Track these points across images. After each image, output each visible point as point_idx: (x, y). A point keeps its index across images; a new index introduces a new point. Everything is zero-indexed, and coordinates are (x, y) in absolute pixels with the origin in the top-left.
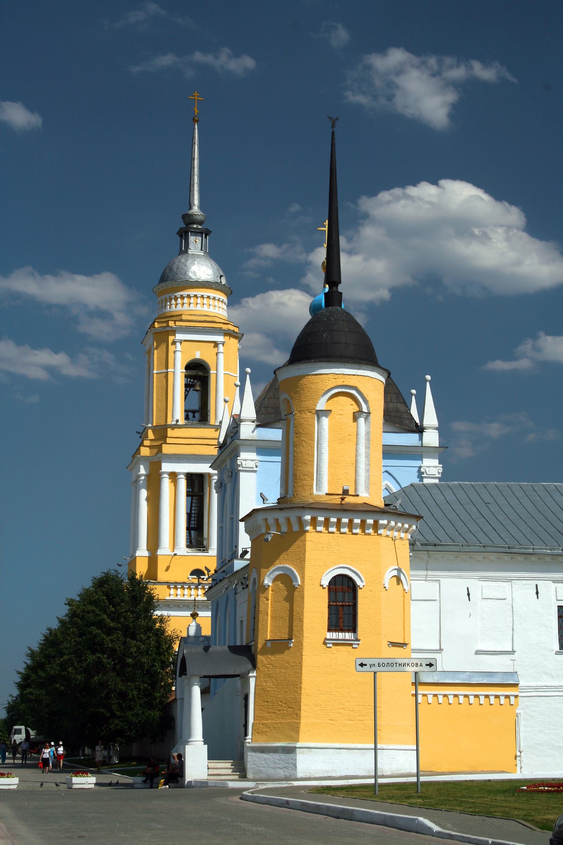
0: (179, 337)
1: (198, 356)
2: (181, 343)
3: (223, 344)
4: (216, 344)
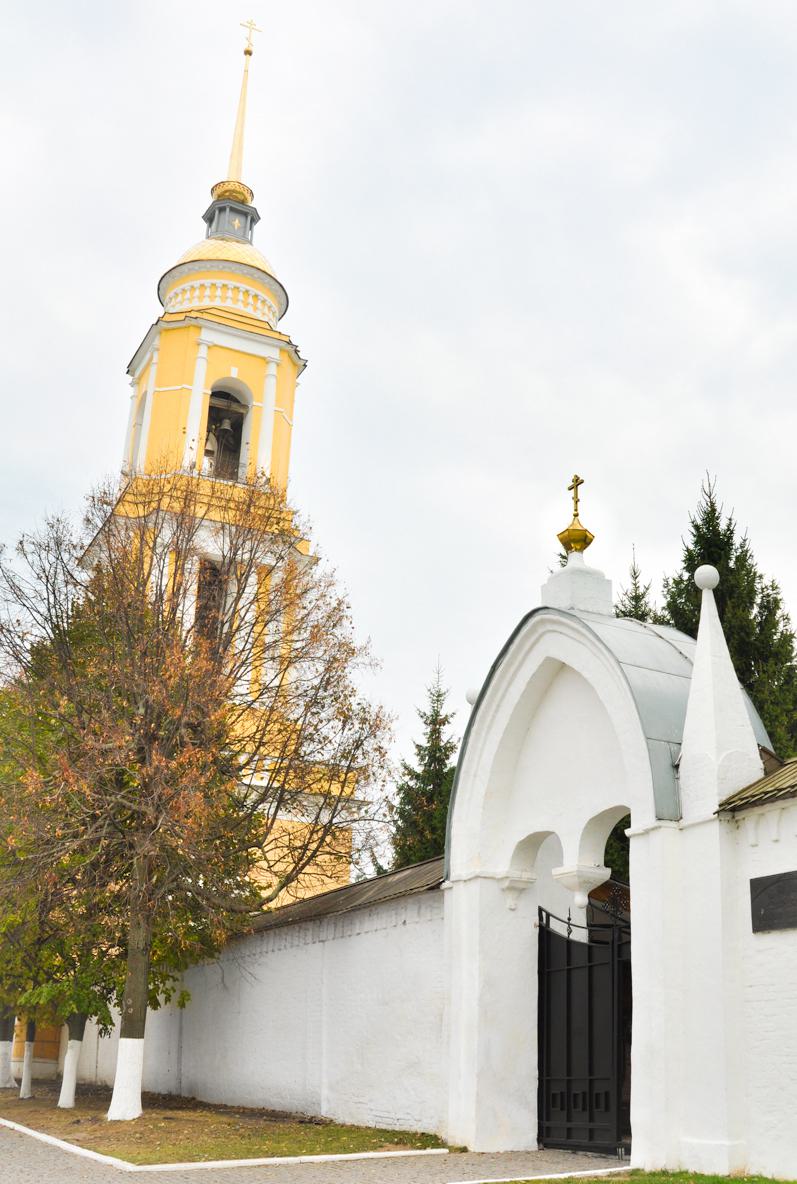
0: (207, 336)
1: (234, 373)
2: (209, 347)
3: (278, 365)
4: (266, 361)
